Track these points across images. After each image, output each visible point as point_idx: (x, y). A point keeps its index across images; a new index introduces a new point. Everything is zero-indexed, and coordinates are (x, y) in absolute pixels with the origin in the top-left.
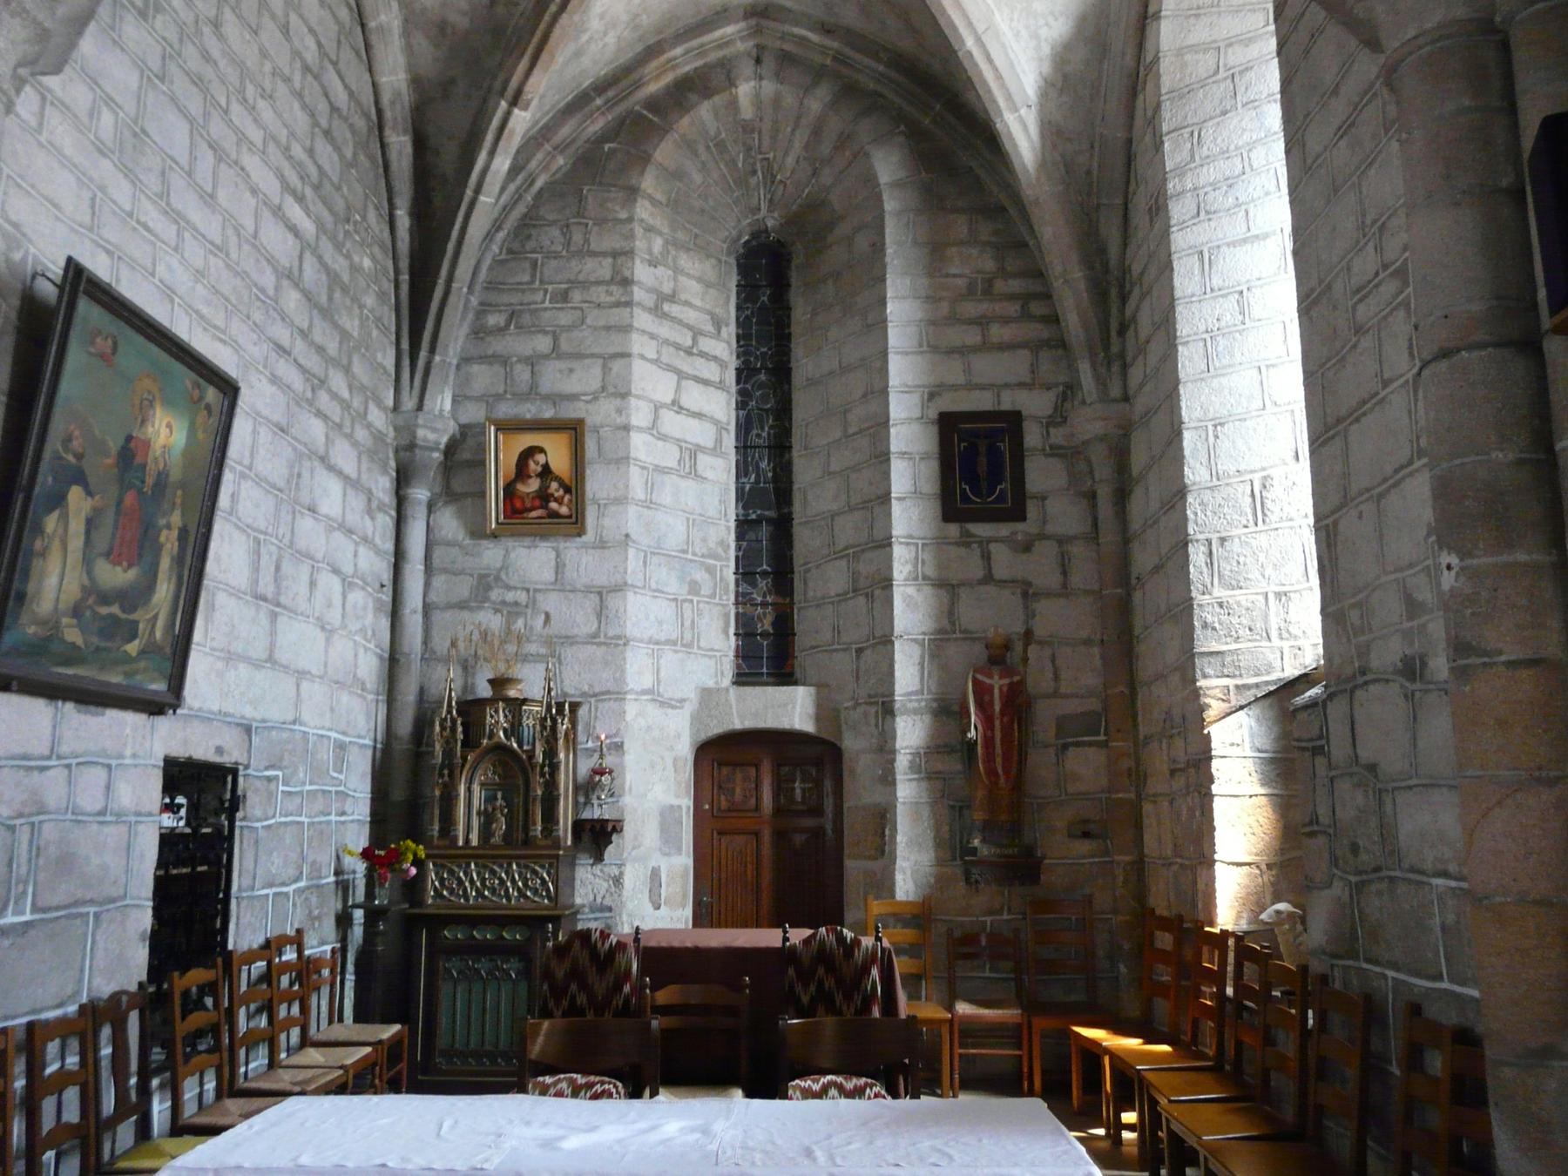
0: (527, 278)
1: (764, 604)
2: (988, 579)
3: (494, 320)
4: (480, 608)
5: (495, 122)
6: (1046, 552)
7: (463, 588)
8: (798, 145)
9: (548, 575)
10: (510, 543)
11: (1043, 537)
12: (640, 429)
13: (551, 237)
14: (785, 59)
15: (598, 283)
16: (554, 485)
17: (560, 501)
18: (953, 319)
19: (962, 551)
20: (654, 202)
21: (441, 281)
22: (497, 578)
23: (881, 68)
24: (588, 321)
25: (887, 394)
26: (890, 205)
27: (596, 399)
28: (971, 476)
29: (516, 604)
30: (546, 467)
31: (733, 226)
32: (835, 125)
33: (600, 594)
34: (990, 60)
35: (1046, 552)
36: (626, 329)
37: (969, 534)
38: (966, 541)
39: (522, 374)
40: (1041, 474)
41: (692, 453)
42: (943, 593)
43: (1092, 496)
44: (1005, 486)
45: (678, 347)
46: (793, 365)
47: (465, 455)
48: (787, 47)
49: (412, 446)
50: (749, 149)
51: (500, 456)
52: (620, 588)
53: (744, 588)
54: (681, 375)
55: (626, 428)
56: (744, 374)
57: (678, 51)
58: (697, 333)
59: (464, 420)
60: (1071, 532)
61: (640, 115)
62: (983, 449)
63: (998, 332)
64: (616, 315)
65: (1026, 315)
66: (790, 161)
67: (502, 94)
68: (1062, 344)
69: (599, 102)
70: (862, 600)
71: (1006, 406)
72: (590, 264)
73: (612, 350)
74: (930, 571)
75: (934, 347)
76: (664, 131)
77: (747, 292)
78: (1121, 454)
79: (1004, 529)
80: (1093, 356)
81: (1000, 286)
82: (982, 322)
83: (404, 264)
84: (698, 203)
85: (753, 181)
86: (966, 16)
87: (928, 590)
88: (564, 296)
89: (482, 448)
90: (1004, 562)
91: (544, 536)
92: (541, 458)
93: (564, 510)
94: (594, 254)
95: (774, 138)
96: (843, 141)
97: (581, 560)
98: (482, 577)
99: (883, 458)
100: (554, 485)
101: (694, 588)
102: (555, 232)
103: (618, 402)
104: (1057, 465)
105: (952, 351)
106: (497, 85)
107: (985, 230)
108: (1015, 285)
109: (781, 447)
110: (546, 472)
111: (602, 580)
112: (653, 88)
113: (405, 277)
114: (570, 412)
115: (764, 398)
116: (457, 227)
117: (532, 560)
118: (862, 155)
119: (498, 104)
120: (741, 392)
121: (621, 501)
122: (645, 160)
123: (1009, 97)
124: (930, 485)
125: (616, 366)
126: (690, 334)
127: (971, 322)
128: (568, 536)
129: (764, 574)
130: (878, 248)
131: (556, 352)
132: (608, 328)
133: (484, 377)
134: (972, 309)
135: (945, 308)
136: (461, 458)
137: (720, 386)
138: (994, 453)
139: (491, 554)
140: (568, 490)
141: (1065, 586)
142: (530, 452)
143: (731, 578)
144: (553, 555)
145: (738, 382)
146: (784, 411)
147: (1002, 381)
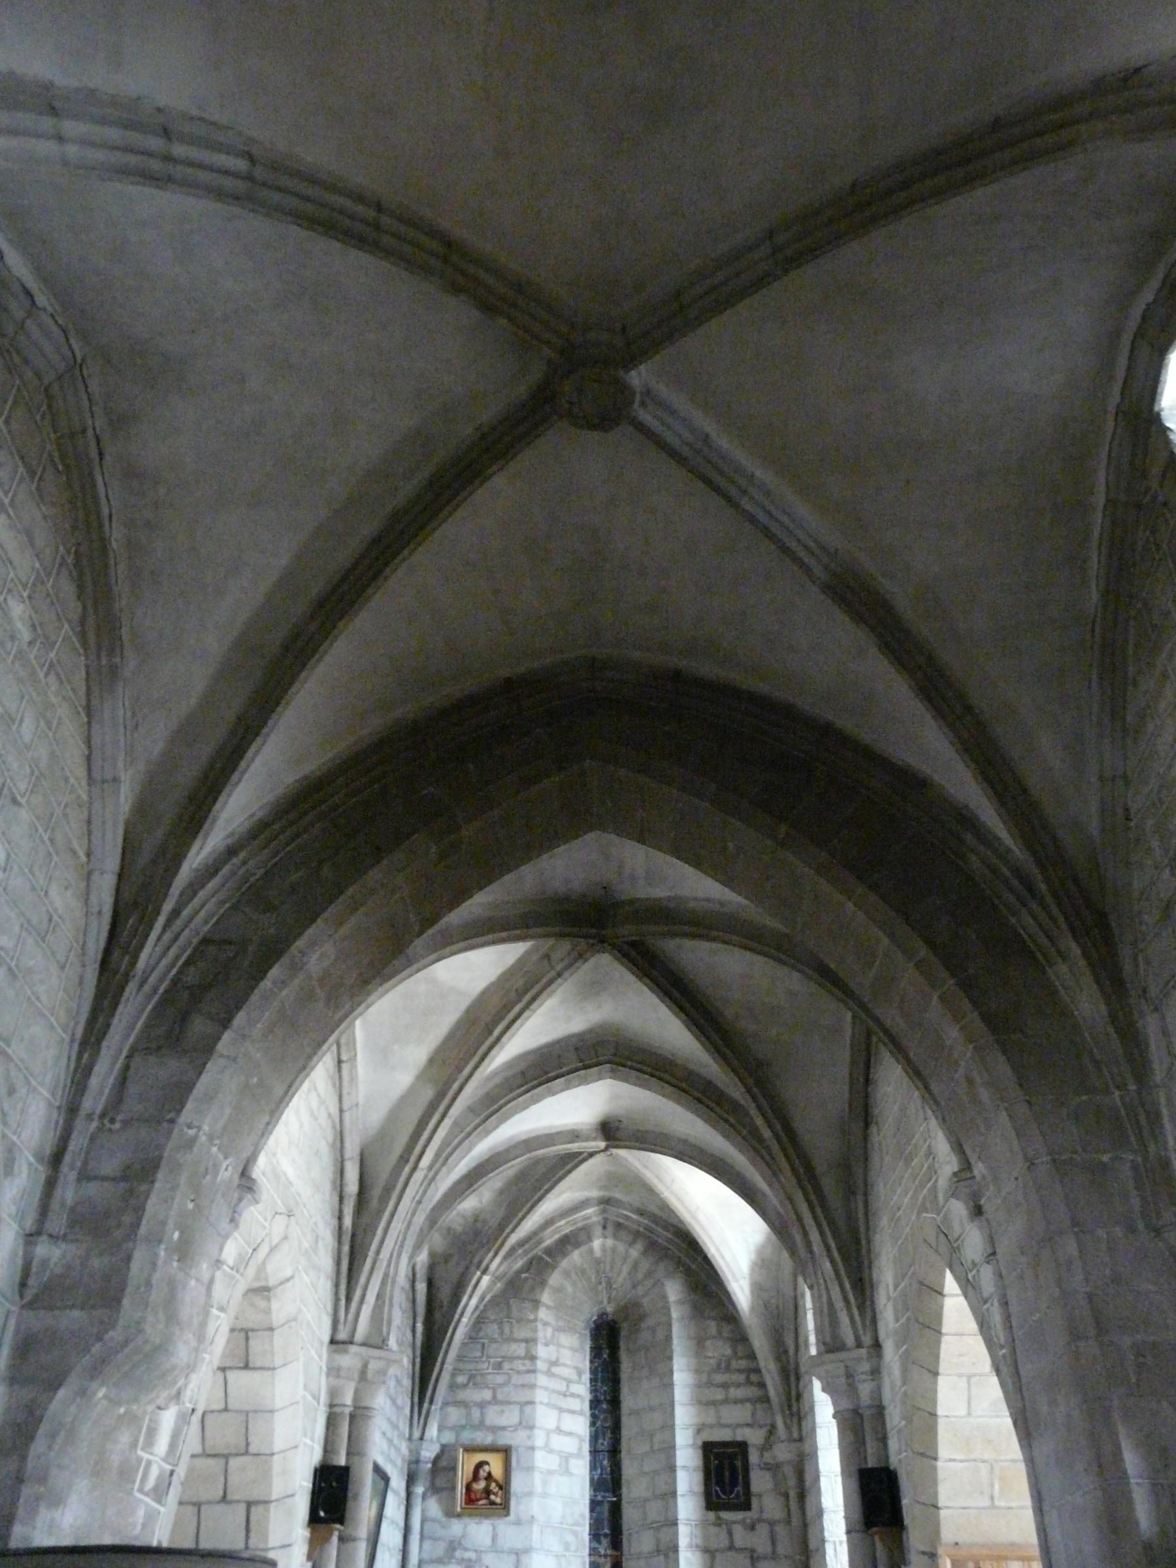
0: (479, 1354)
1: (605, 1556)
2: (731, 1547)
3: (461, 1379)
4: (449, 1563)
5: (473, 1282)
6: (763, 1530)
7: (440, 1550)
8: (624, 1273)
9: (488, 1541)
10: (466, 1520)
11: (760, 1520)
12: (540, 1448)
13: (492, 1329)
14: (619, 1226)
15: (519, 1358)
16: (493, 1485)
17: (496, 1494)
18: (710, 1384)
19: (716, 1529)
20: (548, 1307)
21: (438, 1364)
22: (460, 1543)
23: (669, 1236)
24: (513, 1381)
25: (674, 1430)
26: (675, 1314)
27: (516, 1430)
28: (720, 1482)
29: (470, 1560)
30: (489, 1474)
31: (588, 1312)
32: (645, 1265)
33: (517, 1554)
34: (723, 1257)
35: (763, 1530)
36: (532, 1386)
37: (719, 1518)
38: (718, 1523)
39: (476, 1414)
40: (760, 1482)
41: (566, 1458)
42: (707, 1556)
43: (786, 1496)
44: (739, 1488)
45: (559, 1393)
46: (622, 1398)
47: (443, 1463)
48: (621, 1221)
49: (417, 1462)
50: (598, 1272)
51: (465, 1466)
52: (527, 1551)
53: (596, 1545)
54: (561, 1410)
55: (532, 1448)
56: (594, 1404)
57: (562, 1222)
58: (569, 1382)
59: (444, 1441)
60: (776, 1518)
61: (541, 1258)
62: (726, 1466)
63: (735, 1393)
64: (528, 1378)
65: (749, 1382)
66: (621, 1279)
67: (478, 1268)
68: (766, 1399)
69: (520, 1251)
70: (662, 1558)
71: (739, 1438)
72: (514, 1346)
73: (523, 1399)
74: (699, 1541)
75: (702, 1403)
76: (554, 1267)
77: (596, 1352)
78: (800, 1473)
79: (738, 1516)
80: (783, 1412)
81: (734, 1364)
82: (725, 1386)
83: (418, 1353)
84: (569, 1303)
85: (600, 1288)
86: (709, 1237)
87: (698, 1554)
88: (499, 1366)
89: (455, 1460)
90: (741, 1537)
91: (487, 1517)
92: (486, 1468)
93: (498, 1500)
94: (516, 1340)
95: (612, 1268)
96: (649, 1274)
97: (507, 1531)
98: (451, 1542)
99: (672, 1469)
100: (493, 1485)
101: (567, 1546)
102: (495, 1327)
103: (528, 1432)
104: (768, 1476)
105: (713, 1403)
106: (476, 1261)
107: (727, 1329)
108: (743, 1363)
109: (614, 1451)
110: (489, 1477)
111: (519, 1546)
112: (548, 1242)
113: (418, 1360)
114: (504, 1439)
115: (605, 1420)
116: (449, 1334)
117: (479, 1531)
118: (658, 1283)
119: (475, 1273)
120: (593, 1416)
121: (530, 1494)
122: (543, 1284)
123: (733, 1275)
124: (699, 1487)
125: (528, 1409)
126: (565, 1384)
127: (718, 1386)
128: (500, 1516)
129: (606, 1535)
130: (668, 1339)
131: (495, 1401)
132: (523, 1386)
133: (455, 1415)
134: (719, 1378)
135: (704, 1378)
136: (443, 1466)
137: (581, 1413)
138: (733, 1470)
139: (456, 1527)
140: (501, 1488)
141: (774, 1552)
142: (480, 1465)
143: (586, 1538)
144: (491, 1528)
145: (591, 1408)
146: (616, 1428)
147: (737, 1423)
